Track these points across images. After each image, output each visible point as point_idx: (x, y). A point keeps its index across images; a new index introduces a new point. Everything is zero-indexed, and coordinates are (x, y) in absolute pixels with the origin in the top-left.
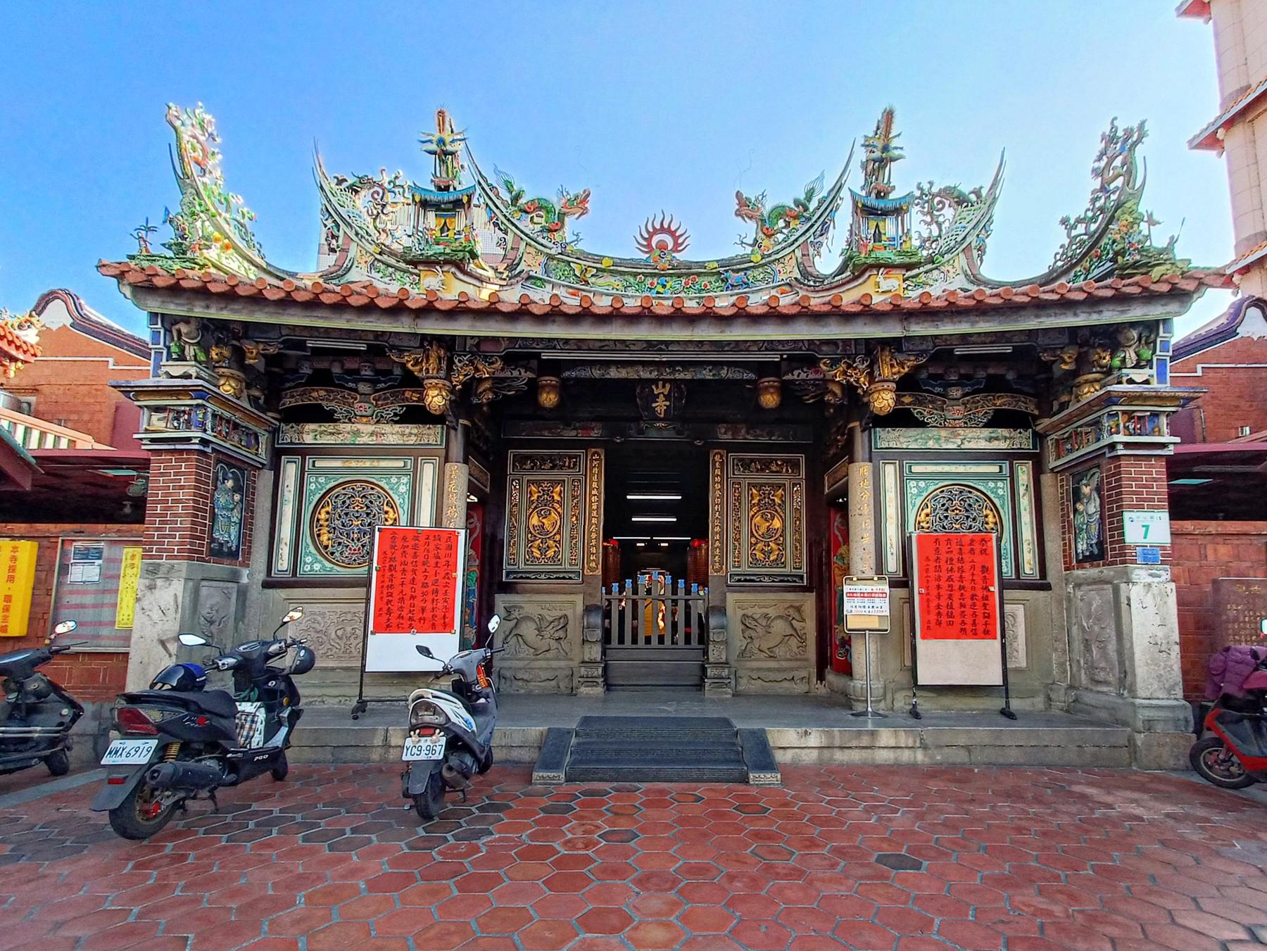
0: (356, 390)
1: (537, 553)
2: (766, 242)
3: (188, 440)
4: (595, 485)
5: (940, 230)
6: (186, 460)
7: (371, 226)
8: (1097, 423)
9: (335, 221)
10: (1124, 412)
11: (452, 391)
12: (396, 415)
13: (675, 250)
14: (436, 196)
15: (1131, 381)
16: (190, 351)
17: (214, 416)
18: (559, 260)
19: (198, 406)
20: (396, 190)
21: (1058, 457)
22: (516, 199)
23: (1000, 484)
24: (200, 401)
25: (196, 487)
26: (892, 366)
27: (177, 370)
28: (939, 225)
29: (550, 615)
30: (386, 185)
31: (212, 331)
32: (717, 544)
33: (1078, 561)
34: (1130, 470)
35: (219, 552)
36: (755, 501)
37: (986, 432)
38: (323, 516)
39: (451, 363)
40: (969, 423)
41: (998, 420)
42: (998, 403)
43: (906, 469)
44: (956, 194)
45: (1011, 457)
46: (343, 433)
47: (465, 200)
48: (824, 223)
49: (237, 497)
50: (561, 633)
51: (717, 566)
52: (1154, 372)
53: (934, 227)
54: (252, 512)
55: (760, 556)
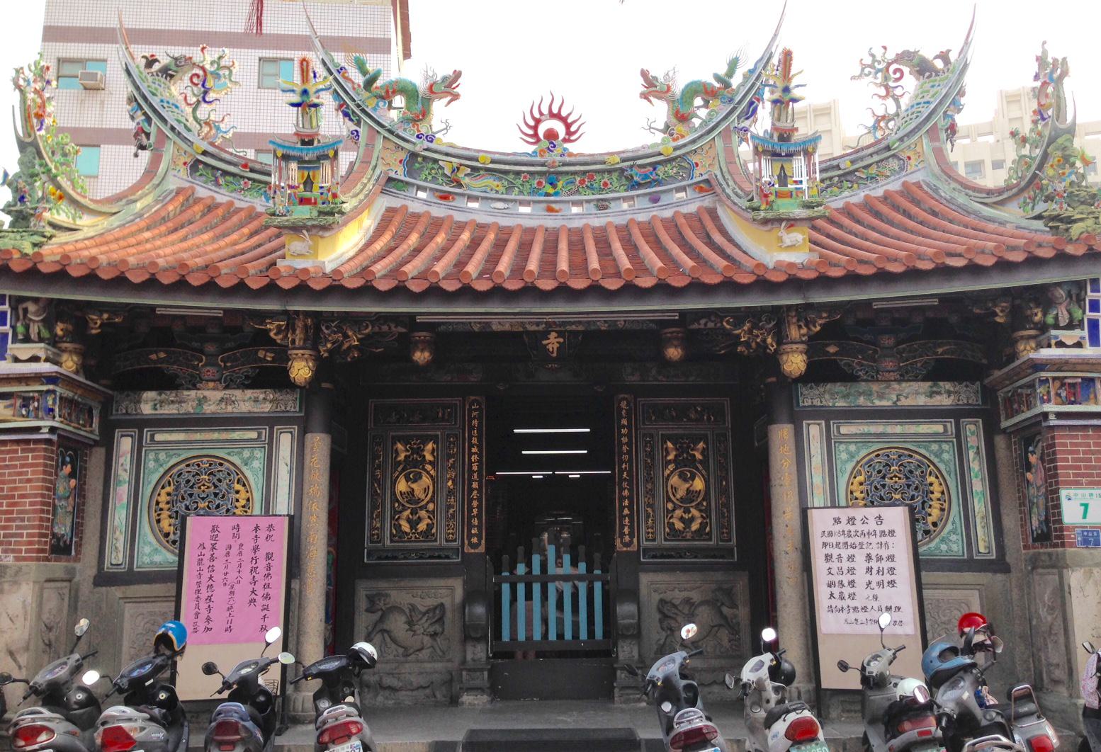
0: (202, 352)
1: (406, 527)
2: (680, 128)
3: (37, 430)
4: (475, 441)
5: (898, 106)
6: (32, 450)
7: (191, 119)
8: (1031, 386)
9: (145, 114)
10: (1054, 379)
11: (318, 359)
12: (247, 377)
13: (565, 140)
14: (299, 150)
15: (1061, 344)
16: (34, 330)
17: (61, 398)
18: (425, 158)
19: (48, 392)
20: (221, 72)
21: (1007, 418)
22: (369, 83)
23: (945, 447)
24: (51, 387)
25: (44, 480)
26: (800, 327)
27: (24, 351)
28: (896, 100)
29: (424, 604)
30: (208, 67)
31: (56, 311)
32: (626, 511)
33: (1034, 540)
34: (1064, 442)
35: (60, 549)
36: (671, 457)
37: (926, 386)
38: (163, 498)
39: (318, 329)
40: (904, 376)
41: (937, 373)
42: (940, 350)
43: (833, 428)
44: (916, 61)
45: (956, 414)
46: (189, 402)
47: (331, 153)
48: (751, 103)
49: (73, 482)
50: (437, 628)
51: (627, 538)
52: (1085, 333)
53: (890, 103)
54: (84, 497)
55: (679, 525)
